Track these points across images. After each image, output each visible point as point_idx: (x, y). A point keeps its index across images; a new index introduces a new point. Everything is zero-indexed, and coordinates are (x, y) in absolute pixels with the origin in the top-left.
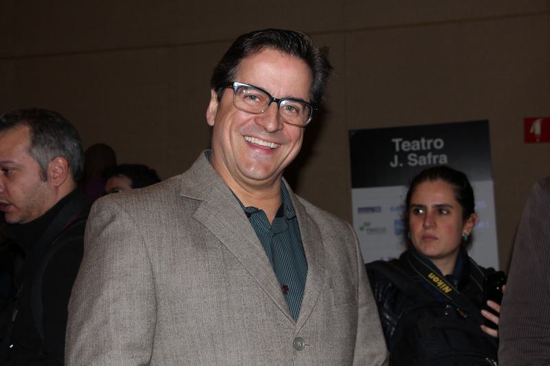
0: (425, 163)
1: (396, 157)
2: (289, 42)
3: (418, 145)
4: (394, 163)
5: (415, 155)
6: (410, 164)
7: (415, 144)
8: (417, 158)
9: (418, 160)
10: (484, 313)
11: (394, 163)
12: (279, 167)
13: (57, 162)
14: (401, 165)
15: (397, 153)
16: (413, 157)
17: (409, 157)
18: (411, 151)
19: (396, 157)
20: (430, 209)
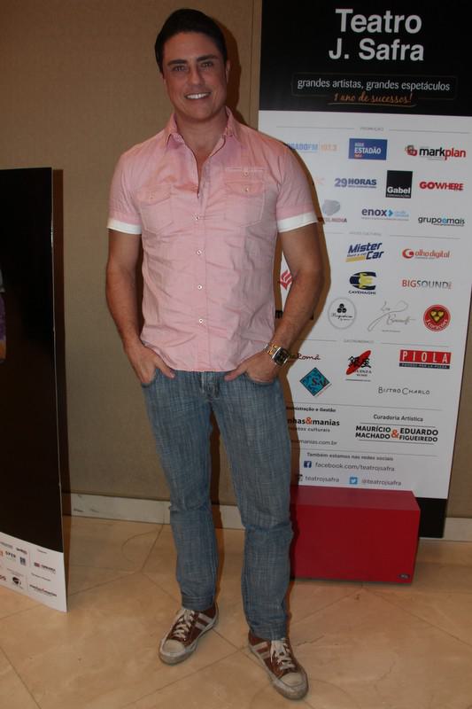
0: (387, 57)
1: (340, 41)
3: (387, 52)
4: (335, 53)
5: (372, 43)
6: (361, 55)
8: (375, 48)
9: (376, 51)
10: (394, 58)
11: (335, 53)
13: (180, 65)
16: (367, 44)
18: (366, 34)
19: (340, 41)
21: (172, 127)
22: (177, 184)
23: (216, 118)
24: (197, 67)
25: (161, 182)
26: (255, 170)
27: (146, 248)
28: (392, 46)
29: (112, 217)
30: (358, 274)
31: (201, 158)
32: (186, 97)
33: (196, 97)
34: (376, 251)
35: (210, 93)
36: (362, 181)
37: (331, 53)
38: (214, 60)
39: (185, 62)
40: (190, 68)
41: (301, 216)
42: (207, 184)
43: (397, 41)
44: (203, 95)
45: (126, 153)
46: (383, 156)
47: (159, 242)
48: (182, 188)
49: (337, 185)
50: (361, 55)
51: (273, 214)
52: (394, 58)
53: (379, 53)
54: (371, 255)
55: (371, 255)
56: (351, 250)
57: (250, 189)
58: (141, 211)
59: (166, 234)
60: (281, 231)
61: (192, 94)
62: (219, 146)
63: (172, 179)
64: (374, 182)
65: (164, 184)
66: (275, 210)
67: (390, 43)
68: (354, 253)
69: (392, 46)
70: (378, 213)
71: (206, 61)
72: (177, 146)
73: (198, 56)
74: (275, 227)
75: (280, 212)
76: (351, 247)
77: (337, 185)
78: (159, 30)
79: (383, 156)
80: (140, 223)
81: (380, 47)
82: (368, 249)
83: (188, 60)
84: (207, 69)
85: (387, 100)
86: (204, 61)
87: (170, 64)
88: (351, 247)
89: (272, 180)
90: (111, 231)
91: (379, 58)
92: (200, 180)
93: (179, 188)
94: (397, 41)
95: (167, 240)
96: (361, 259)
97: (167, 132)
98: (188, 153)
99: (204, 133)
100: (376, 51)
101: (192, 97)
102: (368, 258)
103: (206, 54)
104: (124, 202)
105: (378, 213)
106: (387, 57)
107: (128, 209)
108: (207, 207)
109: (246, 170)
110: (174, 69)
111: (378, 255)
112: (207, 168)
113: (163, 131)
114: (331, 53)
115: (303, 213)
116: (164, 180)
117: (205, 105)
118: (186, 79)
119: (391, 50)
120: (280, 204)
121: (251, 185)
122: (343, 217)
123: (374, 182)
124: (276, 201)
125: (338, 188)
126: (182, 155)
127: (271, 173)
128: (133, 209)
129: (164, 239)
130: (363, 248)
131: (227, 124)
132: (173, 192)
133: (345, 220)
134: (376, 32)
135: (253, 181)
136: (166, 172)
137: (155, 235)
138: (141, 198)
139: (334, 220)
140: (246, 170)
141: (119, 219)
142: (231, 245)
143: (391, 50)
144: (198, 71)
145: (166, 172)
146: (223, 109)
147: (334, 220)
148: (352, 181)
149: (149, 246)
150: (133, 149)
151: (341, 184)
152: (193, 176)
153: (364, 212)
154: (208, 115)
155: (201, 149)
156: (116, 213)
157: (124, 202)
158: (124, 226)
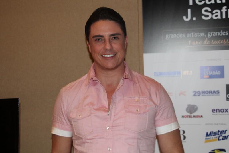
0: (219, 17)
1: (189, 11)
2: (194, 21)
3: (219, 14)
4: (187, 18)
5: (209, 10)
6: (203, 17)
7: (217, 13)
8: (211, 12)
9: (212, 14)
10: (224, 17)
11: (187, 18)
12: (139, 83)
13: (99, 38)
14: (194, 19)
15: (190, 7)
16: (206, 11)
17: (203, 12)
18: (205, 5)
19: (189, 11)
20: (107, 37)
21: (92, 73)
22: (95, 107)
23: (119, 68)
24: (109, 39)
25: (85, 106)
26: (142, 98)
27: (75, 146)
28: (222, 11)
29: (55, 126)
30: (214, 150)
31: (111, 92)
32: (102, 56)
33: (108, 56)
34: (224, 135)
35: (116, 54)
36: (210, 92)
37: (185, 18)
38: (119, 36)
39: (102, 36)
40: (105, 40)
41: (170, 125)
42: (114, 107)
43: (225, 7)
44: (112, 55)
45: (64, 88)
46: (222, 76)
47: (84, 143)
48: (98, 109)
49: (194, 95)
50: (203, 17)
51: (154, 124)
52: (224, 17)
53: (214, 16)
54: (221, 138)
55: (221, 138)
56: (207, 135)
57: (140, 110)
58: (73, 123)
59: (88, 138)
60: (158, 134)
61: (106, 54)
62: (121, 84)
63: (92, 104)
64: (218, 92)
65: (87, 106)
66: (155, 121)
67: (220, 9)
68: (209, 137)
69: (222, 11)
70: (222, 111)
71: (115, 36)
72: (95, 84)
73: (111, 33)
74: (154, 131)
75: (158, 123)
76: (207, 133)
77: (194, 95)
78: (88, 18)
79: (222, 76)
80: (72, 130)
81: (214, 12)
82: (218, 134)
83: (104, 35)
84: (115, 41)
85: (221, 42)
86: (114, 36)
87: (94, 37)
88: (207, 133)
89: (152, 103)
90: (53, 135)
91: (214, 18)
92: (109, 105)
93: (96, 110)
94: (225, 7)
95: (89, 141)
96: (215, 140)
97: (89, 75)
98: (102, 90)
99: (113, 76)
100: (212, 14)
101: (106, 56)
102: (219, 140)
103: (115, 33)
104: (62, 117)
105: (222, 111)
106: (219, 17)
107: (64, 121)
108: (114, 121)
109: (137, 98)
110: (96, 40)
111: (225, 138)
112: (114, 97)
113: (86, 76)
114: (185, 18)
115: (171, 122)
116: (88, 105)
117: (113, 61)
118: (103, 46)
119: (222, 13)
120: (157, 118)
121: (140, 107)
122: (200, 114)
123: (218, 92)
124: (155, 116)
125: (195, 97)
126: (98, 90)
127: (151, 100)
128: (68, 121)
129: (87, 141)
130: (215, 134)
131: (125, 71)
132: (92, 112)
133: (202, 117)
134: (211, 4)
135: (141, 105)
136: (88, 100)
137: (81, 138)
138: (73, 115)
139: (194, 117)
140: (137, 98)
141: (59, 128)
142: (129, 145)
143: (222, 13)
144: (110, 42)
145: (88, 100)
146: (122, 63)
147: (194, 117)
148: (204, 92)
149: (78, 145)
150: (68, 86)
151: (197, 94)
152: (105, 103)
153: (213, 111)
154: (114, 66)
155: (109, 86)
156: (57, 124)
157: (62, 117)
158: (61, 131)
